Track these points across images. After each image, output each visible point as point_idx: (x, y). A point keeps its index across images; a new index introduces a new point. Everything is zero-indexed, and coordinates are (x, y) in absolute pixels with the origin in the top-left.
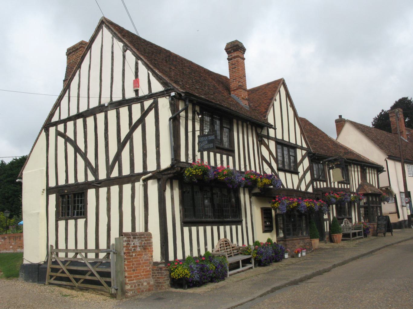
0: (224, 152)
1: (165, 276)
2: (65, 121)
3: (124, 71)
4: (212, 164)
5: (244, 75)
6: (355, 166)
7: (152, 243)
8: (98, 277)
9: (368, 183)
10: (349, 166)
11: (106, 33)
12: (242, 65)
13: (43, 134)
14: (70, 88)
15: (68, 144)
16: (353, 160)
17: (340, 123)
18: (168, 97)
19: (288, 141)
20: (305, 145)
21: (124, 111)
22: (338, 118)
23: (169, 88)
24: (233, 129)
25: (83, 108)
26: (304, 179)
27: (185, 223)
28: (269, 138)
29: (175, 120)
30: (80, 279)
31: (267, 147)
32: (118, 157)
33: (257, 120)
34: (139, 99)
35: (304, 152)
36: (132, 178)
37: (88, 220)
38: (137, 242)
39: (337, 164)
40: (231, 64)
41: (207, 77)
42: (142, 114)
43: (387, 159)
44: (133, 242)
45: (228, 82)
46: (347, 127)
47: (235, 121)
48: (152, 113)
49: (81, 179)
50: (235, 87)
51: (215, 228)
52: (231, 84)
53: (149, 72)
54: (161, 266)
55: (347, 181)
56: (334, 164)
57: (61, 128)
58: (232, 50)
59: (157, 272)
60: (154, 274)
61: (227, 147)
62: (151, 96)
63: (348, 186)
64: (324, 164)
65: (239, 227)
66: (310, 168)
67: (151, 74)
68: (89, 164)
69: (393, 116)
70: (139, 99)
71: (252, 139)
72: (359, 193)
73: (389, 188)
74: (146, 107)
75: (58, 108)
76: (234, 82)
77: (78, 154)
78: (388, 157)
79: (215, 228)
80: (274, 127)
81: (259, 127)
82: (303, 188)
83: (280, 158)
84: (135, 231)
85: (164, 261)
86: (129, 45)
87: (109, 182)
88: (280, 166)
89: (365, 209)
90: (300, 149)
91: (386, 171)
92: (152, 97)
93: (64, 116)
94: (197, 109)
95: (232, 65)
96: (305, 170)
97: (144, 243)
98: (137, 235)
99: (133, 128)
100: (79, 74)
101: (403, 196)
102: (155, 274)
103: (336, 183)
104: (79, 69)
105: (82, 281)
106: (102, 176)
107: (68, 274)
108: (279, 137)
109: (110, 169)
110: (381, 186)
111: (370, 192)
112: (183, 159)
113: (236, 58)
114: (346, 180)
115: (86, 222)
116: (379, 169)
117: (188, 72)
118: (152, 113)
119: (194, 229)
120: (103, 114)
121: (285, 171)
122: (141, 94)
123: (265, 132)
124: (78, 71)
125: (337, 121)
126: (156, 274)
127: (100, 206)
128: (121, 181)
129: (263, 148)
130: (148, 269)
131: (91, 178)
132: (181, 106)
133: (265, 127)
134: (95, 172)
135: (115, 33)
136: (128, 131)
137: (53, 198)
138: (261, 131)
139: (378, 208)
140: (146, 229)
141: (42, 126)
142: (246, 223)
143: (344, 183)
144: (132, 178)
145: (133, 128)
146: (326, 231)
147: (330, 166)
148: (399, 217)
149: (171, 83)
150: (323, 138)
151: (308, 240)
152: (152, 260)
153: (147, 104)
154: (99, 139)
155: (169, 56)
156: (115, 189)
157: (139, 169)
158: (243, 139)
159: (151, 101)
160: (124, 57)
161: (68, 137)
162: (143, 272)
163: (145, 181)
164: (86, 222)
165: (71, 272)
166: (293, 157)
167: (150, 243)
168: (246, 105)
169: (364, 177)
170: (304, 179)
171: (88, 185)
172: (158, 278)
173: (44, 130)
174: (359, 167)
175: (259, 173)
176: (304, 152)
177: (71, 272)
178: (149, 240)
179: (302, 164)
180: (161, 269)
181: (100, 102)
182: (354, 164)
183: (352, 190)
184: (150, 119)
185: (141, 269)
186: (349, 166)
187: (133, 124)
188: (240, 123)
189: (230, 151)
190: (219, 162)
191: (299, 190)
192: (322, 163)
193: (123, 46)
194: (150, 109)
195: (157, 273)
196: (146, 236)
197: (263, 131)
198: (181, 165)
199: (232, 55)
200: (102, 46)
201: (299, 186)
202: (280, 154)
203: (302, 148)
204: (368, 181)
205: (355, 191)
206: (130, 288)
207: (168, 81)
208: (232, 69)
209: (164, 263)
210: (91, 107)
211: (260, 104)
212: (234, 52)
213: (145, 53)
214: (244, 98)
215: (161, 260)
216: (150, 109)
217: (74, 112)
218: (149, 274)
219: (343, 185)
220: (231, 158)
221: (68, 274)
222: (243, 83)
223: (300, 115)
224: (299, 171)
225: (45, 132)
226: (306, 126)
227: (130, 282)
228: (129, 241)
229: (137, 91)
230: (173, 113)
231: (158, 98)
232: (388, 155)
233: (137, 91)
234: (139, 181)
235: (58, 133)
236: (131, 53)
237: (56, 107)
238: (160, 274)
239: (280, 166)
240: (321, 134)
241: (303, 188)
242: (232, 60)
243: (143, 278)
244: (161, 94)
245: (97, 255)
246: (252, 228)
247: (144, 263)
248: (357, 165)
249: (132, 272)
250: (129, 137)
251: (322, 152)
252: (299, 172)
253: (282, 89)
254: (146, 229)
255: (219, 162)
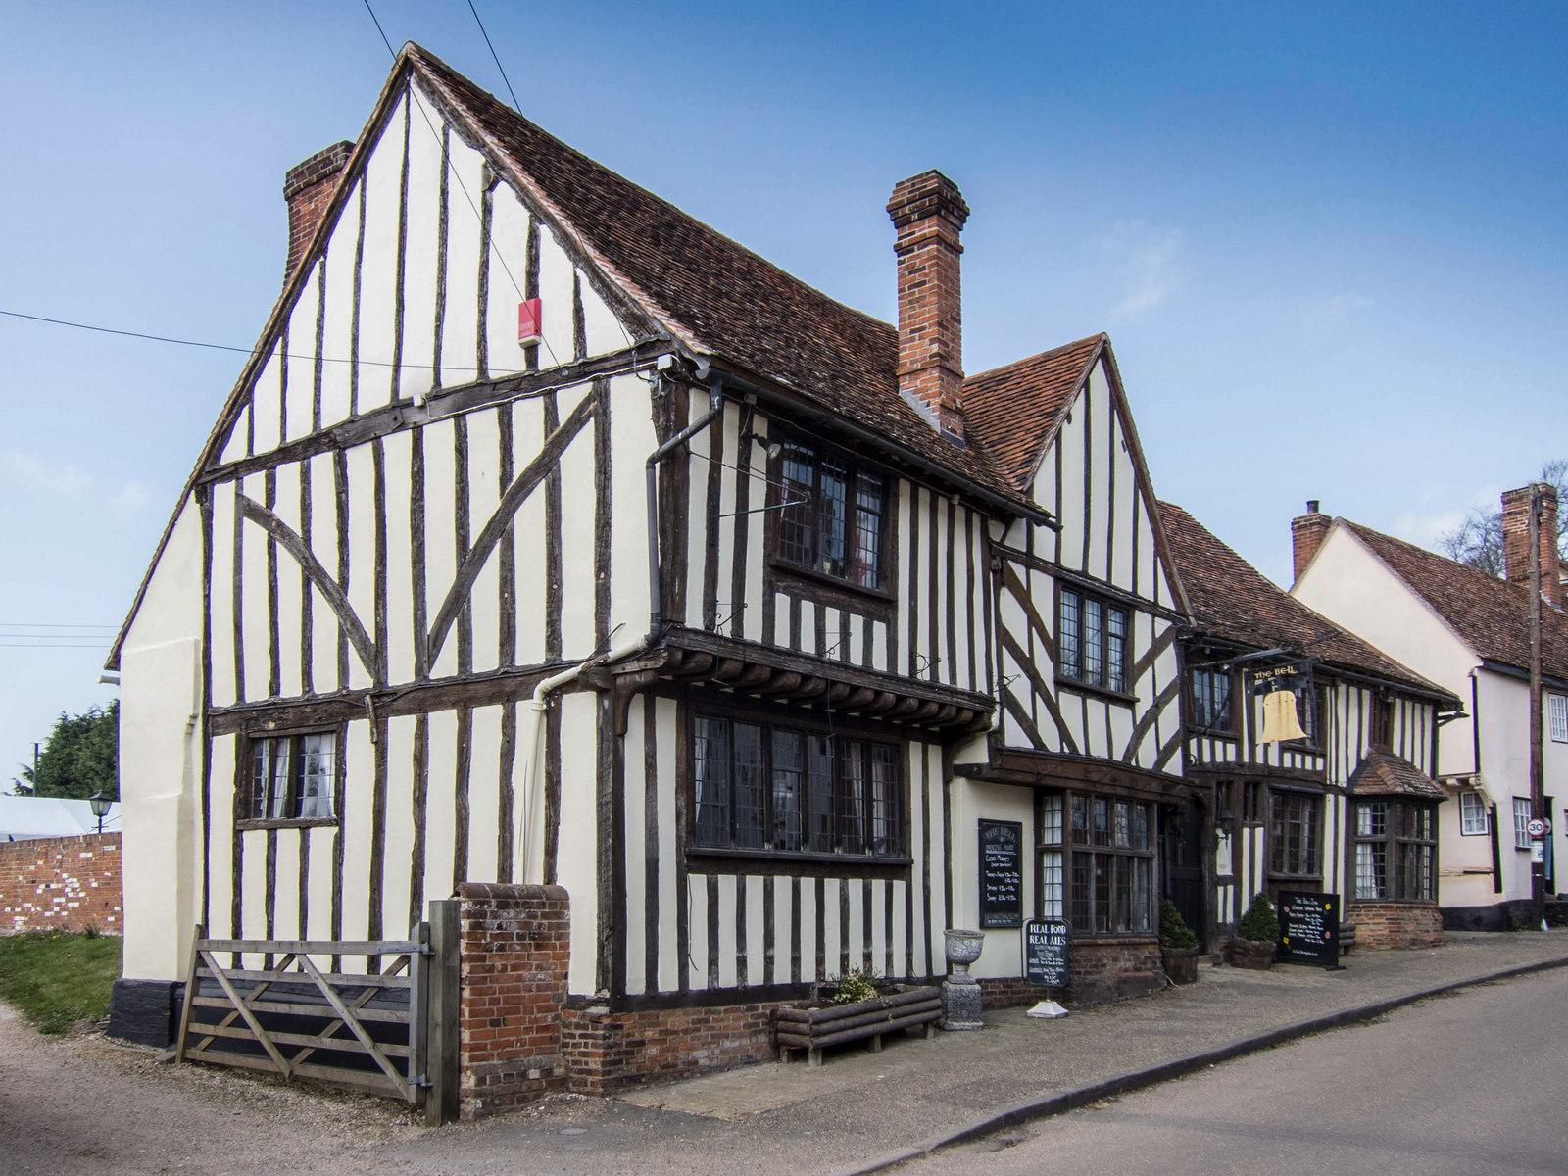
0: (857, 603)
1: (608, 1050)
2: (266, 463)
3: (487, 267)
4: (808, 646)
5: (954, 314)
6: (1353, 691)
7: (568, 925)
8: (364, 1042)
9: (1393, 755)
10: (1328, 689)
11: (422, 116)
12: (949, 274)
13: (193, 507)
14: (287, 333)
15: (281, 549)
16: (1348, 667)
17: (1311, 531)
18: (646, 375)
19: (1104, 579)
20: (1166, 601)
21: (483, 424)
22: (1304, 512)
23: (653, 338)
24: (896, 516)
25: (335, 414)
26: (1153, 725)
27: (692, 860)
28: (1030, 561)
29: (671, 464)
30: (300, 1048)
31: (1024, 598)
32: (458, 602)
33: (990, 489)
34: (537, 382)
35: (1162, 626)
36: (507, 686)
37: (346, 831)
38: (511, 919)
39: (1287, 676)
40: (907, 268)
41: (815, 318)
42: (549, 439)
43: (1476, 673)
44: (498, 922)
45: (895, 347)
46: (1339, 542)
47: (905, 488)
48: (585, 439)
49: (326, 683)
50: (917, 361)
51: (808, 884)
52: (905, 349)
53: (579, 271)
54: (594, 1010)
55: (1316, 743)
56: (1273, 675)
57: (254, 486)
58: (913, 212)
59: (578, 1032)
60: (568, 1040)
61: (869, 586)
62: (585, 369)
63: (1320, 761)
64: (1233, 676)
65: (899, 886)
66: (1182, 686)
67: (587, 280)
68: (352, 625)
69: (1516, 513)
70: (537, 382)
71: (965, 554)
72: (1358, 790)
73: (1472, 781)
74: (563, 417)
75: (246, 410)
76: (913, 340)
77: (314, 588)
78: (1481, 664)
79: (808, 884)
80: (1054, 521)
81: (996, 510)
82: (1146, 758)
83: (1068, 642)
84: (510, 881)
85: (608, 996)
86: (508, 161)
87: (424, 698)
88: (1068, 671)
89: (1374, 849)
90: (1148, 612)
91: (1466, 716)
92: (586, 375)
93: (267, 443)
94: (760, 426)
95: (910, 273)
96: (1158, 694)
97: (540, 925)
98: (514, 897)
99: (513, 495)
100: (320, 279)
101: (1525, 811)
102: (572, 1041)
103: (1274, 752)
104: (322, 259)
105: (305, 1054)
106: (401, 671)
107: (256, 1031)
108: (1072, 561)
109: (427, 648)
110: (1442, 771)
111: (1400, 789)
112: (694, 619)
113: (926, 246)
114: (1313, 738)
115: (339, 841)
116: (1439, 704)
117: (738, 289)
118: (587, 435)
119: (727, 883)
120: (406, 437)
121: (1085, 692)
122: (545, 363)
123: (1016, 540)
124: (318, 265)
125: (1298, 526)
126: (577, 1040)
127: (389, 783)
128: (465, 693)
129: (1007, 599)
130: (549, 1019)
131: (361, 679)
132: (698, 406)
133: (1023, 518)
134: (376, 656)
135: (454, 113)
136: (496, 503)
137: (225, 746)
138: (1005, 536)
139: (1426, 850)
140: (550, 874)
141: (186, 480)
142: (926, 874)
143: (1304, 752)
144: (507, 686)
145: (513, 495)
146: (1220, 920)
147: (1258, 682)
148: (1498, 888)
149: (659, 317)
150: (1243, 581)
151: (1151, 948)
152: (566, 987)
153: (570, 399)
154: (385, 531)
155: (671, 226)
156: (444, 723)
157: (531, 651)
158: (932, 552)
159: (584, 389)
160: (487, 210)
161: (280, 524)
162: (528, 1030)
163: (553, 695)
164: (339, 841)
165: (269, 1021)
166: (1118, 641)
167: (560, 926)
168: (952, 431)
169: (1381, 733)
170: (1153, 725)
171: (346, 706)
172: (584, 1054)
173: (193, 492)
174: (1366, 694)
175: (985, 692)
176: (1162, 626)
177: (269, 1021)
178: (559, 915)
179: (1150, 668)
180: (596, 1020)
181: (395, 391)
182: (1349, 682)
183: (1333, 779)
184: (578, 460)
185: (520, 1021)
186: (1328, 689)
187: (515, 479)
188: (924, 495)
189: (880, 605)
190: (832, 639)
191: (1133, 763)
192: (1226, 673)
193: (485, 166)
194: (577, 421)
195: (582, 1036)
196: (551, 903)
197: (1011, 534)
198: (685, 642)
199: (914, 233)
200: (406, 164)
201: (1132, 750)
202: (1069, 627)
203: (1154, 609)
204: (1396, 751)
205: (1342, 782)
206: (476, 1085)
207: (650, 310)
208: (910, 289)
209: (606, 1000)
210: (362, 410)
211: (1007, 432)
212: (920, 219)
213: (568, 199)
214: (948, 405)
215: (598, 991)
216: (577, 421)
217: (300, 429)
218: (551, 1038)
219: (1298, 757)
220: (879, 629)
221: (256, 1031)
222: (947, 345)
223: (1161, 494)
224: (1137, 696)
225: (197, 501)
226: (1178, 537)
227: (476, 1064)
228: (483, 915)
229: (531, 350)
230: (662, 439)
231: (610, 377)
232: (1482, 658)
233: (531, 350)
234: (530, 696)
235: (246, 509)
236: (513, 194)
237: (237, 407)
238: (590, 1041)
239: (1068, 671)
240: (1231, 567)
241: (1146, 758)
242: (913, 251)
243: (529, 1053)
244: (622, 363)
245: (374, 963)
246: (944, 892)
247: (534, 999)
248: (1361, 685)
249: (489, 1028)
250: (501, 528)
251: (1224, 627)
252: (1138, 700)
253: (1098, 378)
254: (550, 874)
255: (832, 639)
